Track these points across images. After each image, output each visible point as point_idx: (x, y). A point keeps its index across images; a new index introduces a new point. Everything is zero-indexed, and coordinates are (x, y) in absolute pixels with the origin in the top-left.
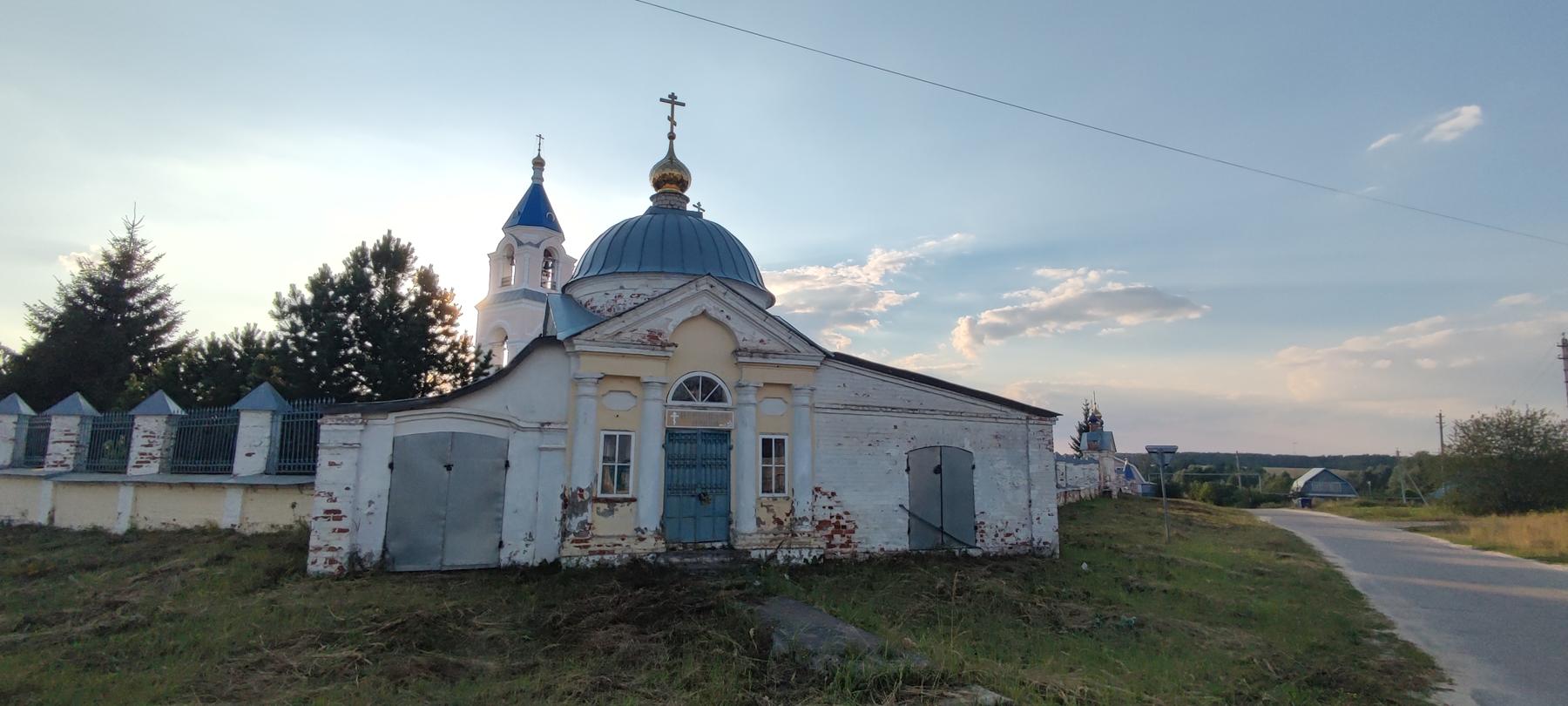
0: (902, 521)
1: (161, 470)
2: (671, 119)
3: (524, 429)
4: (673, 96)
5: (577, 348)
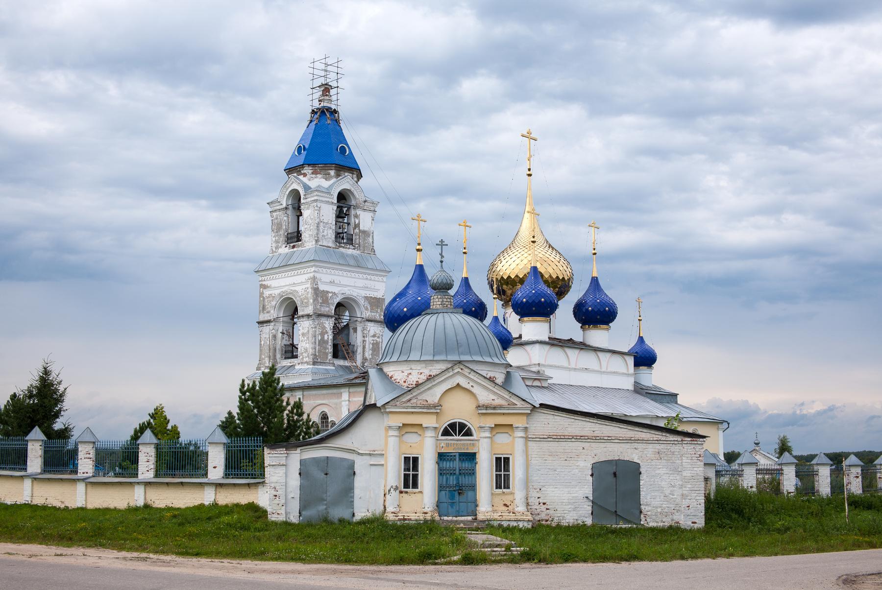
0: (588, 508)
1: (152, 476)
2: (442, 257)
3: (362, 454)
4: (442, 241)
5: (388, 410)
